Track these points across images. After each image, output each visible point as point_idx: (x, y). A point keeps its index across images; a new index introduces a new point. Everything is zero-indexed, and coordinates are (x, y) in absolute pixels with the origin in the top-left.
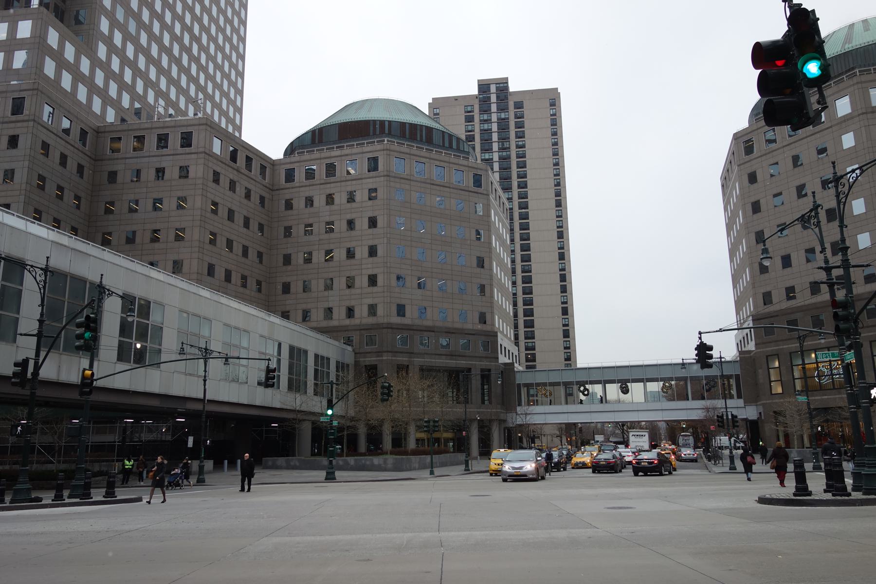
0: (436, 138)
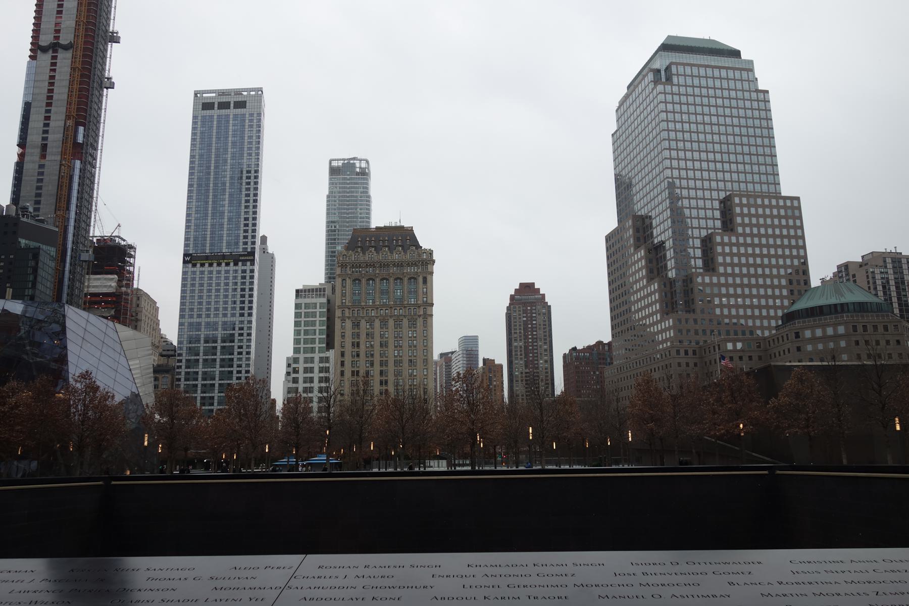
0: (851, 307)
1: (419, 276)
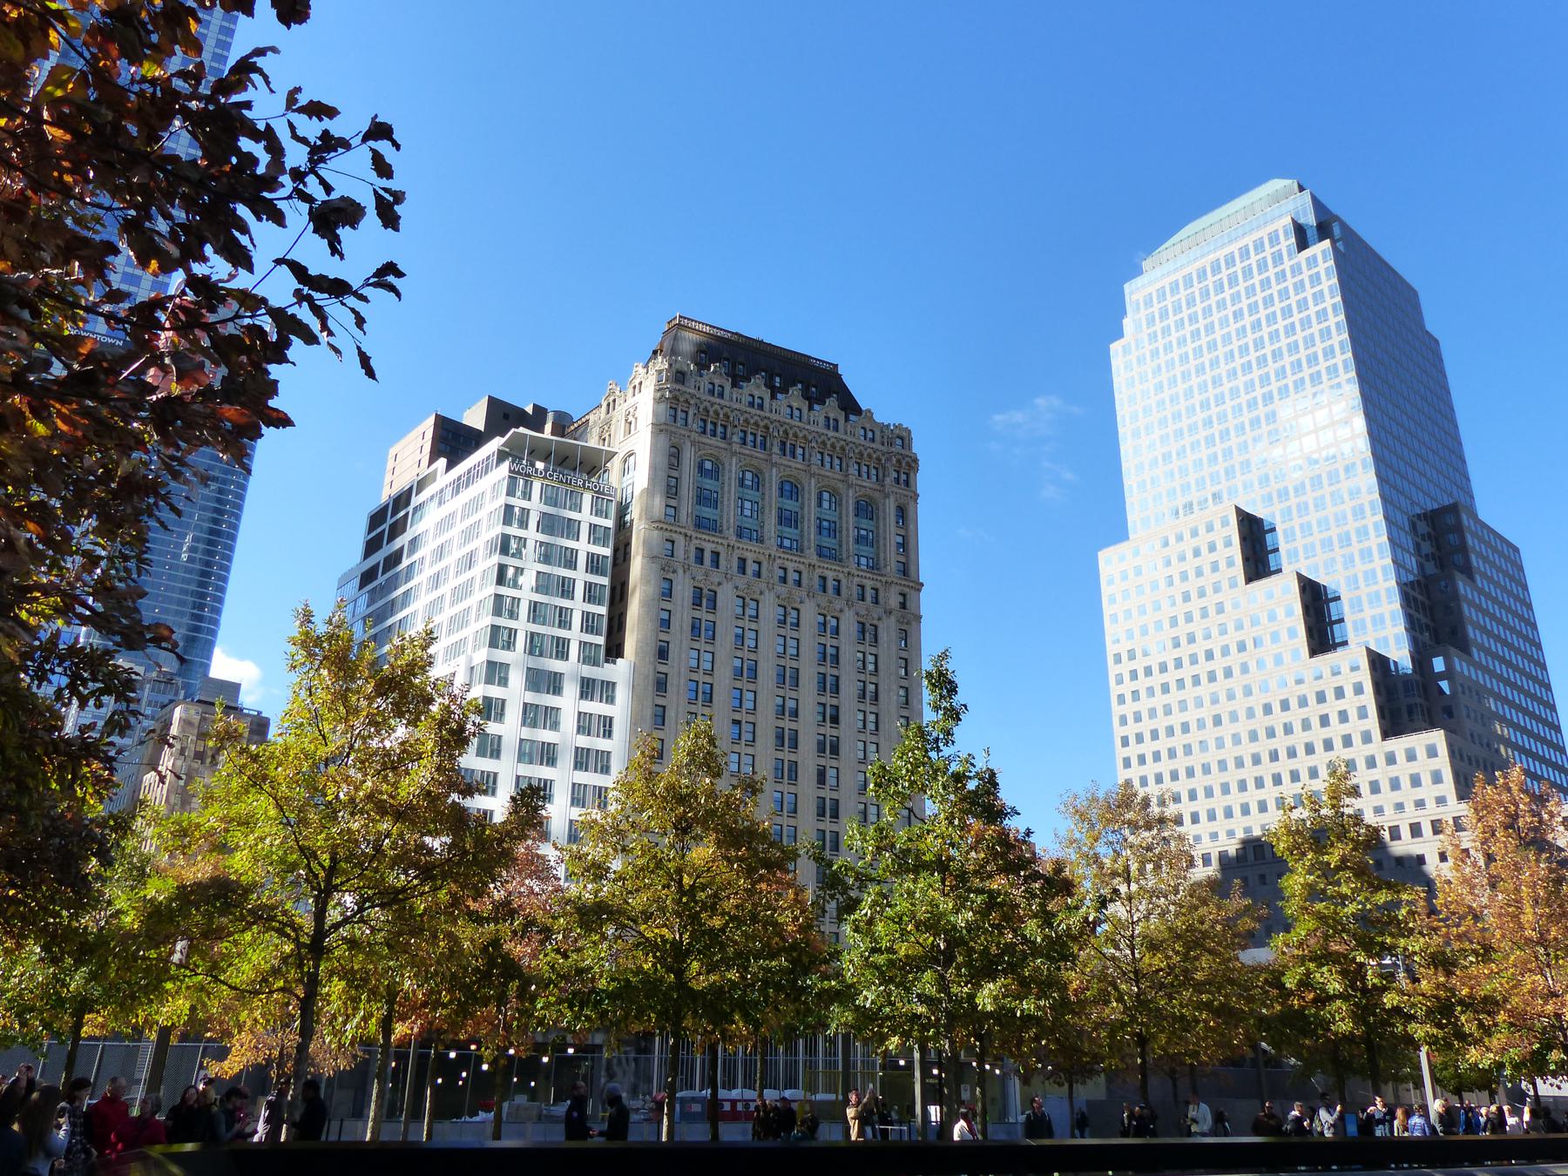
1: (887, 496)
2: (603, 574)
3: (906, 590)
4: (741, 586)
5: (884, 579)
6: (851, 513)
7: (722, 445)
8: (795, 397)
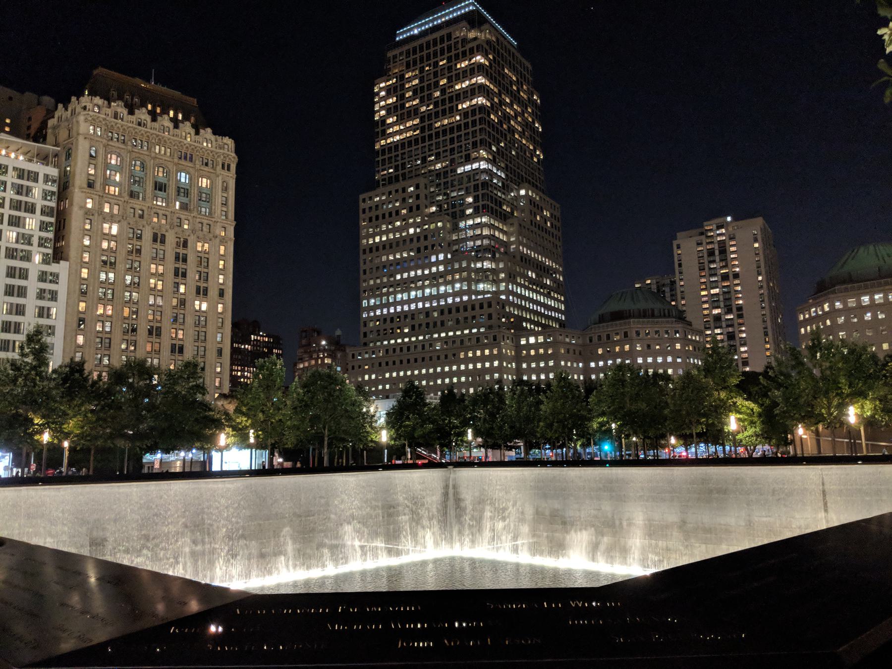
1: (218, 176)
2: (52, 216)
3: (226, 225)
4: (132, 223)
5: (213, 220)
6: (220, 190)
7: (122, 146)
8: (142, 114)
